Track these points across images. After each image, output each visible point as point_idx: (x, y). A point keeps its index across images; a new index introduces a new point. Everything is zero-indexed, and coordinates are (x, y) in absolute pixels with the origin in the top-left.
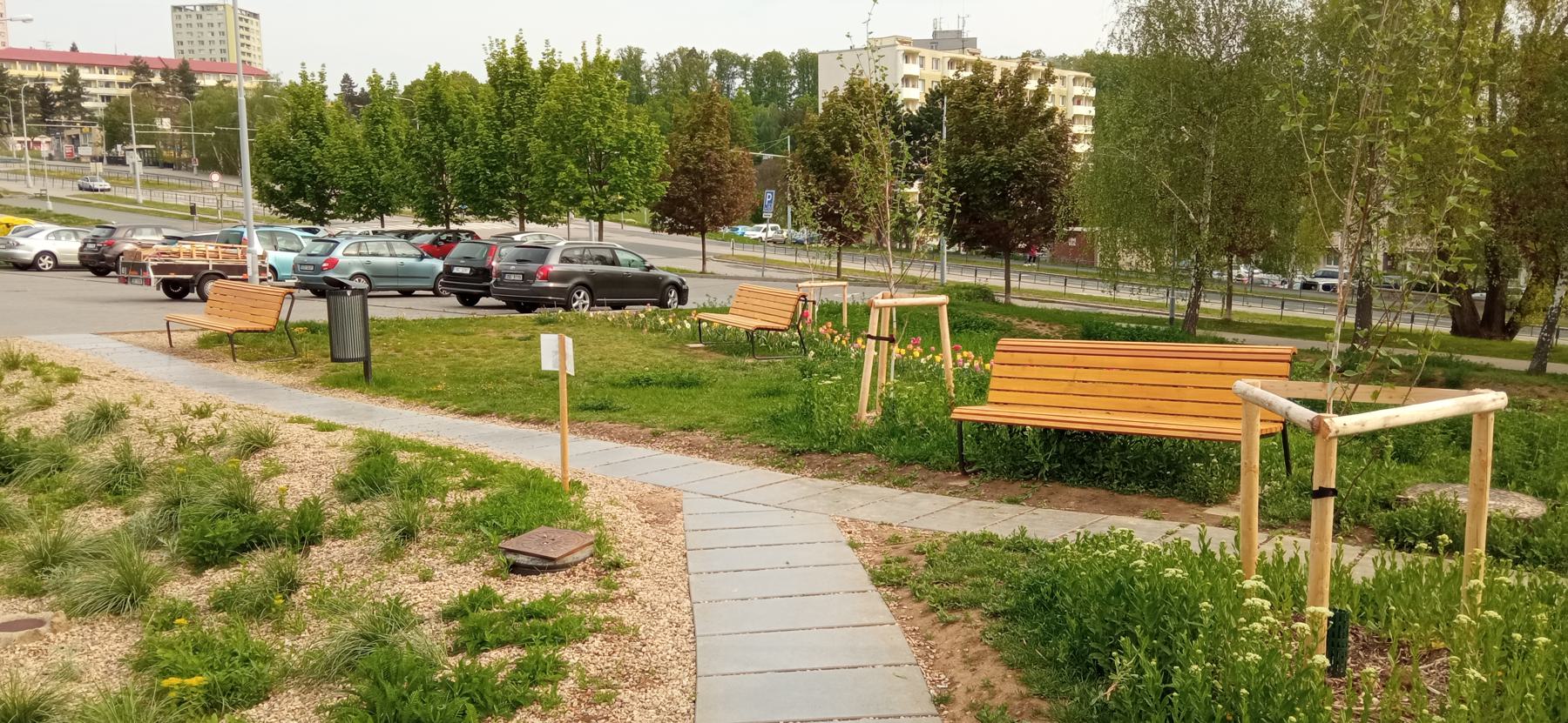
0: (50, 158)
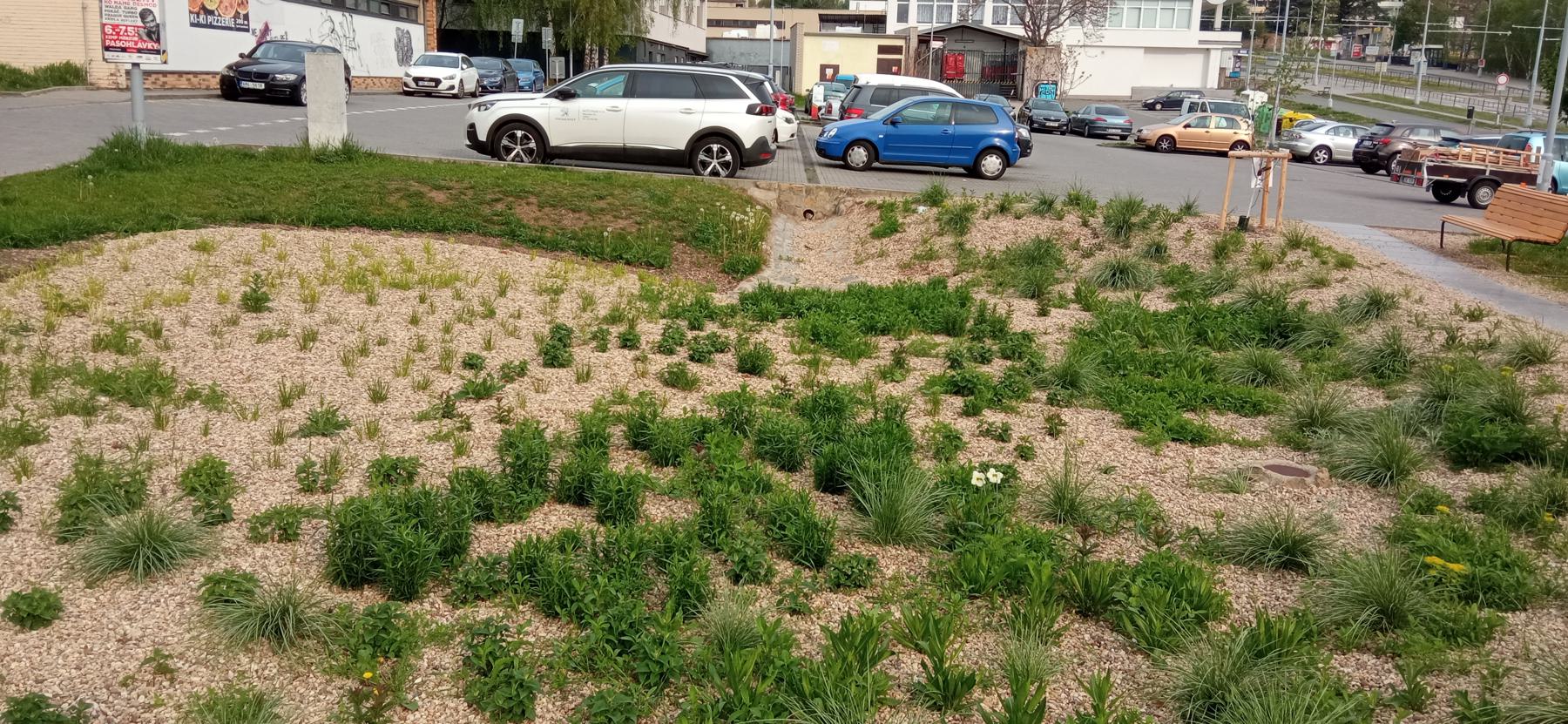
0: (1339, 57)
